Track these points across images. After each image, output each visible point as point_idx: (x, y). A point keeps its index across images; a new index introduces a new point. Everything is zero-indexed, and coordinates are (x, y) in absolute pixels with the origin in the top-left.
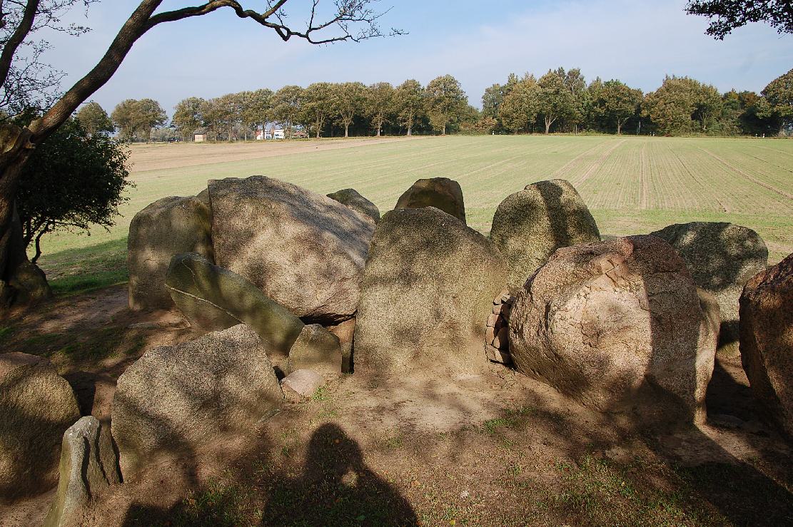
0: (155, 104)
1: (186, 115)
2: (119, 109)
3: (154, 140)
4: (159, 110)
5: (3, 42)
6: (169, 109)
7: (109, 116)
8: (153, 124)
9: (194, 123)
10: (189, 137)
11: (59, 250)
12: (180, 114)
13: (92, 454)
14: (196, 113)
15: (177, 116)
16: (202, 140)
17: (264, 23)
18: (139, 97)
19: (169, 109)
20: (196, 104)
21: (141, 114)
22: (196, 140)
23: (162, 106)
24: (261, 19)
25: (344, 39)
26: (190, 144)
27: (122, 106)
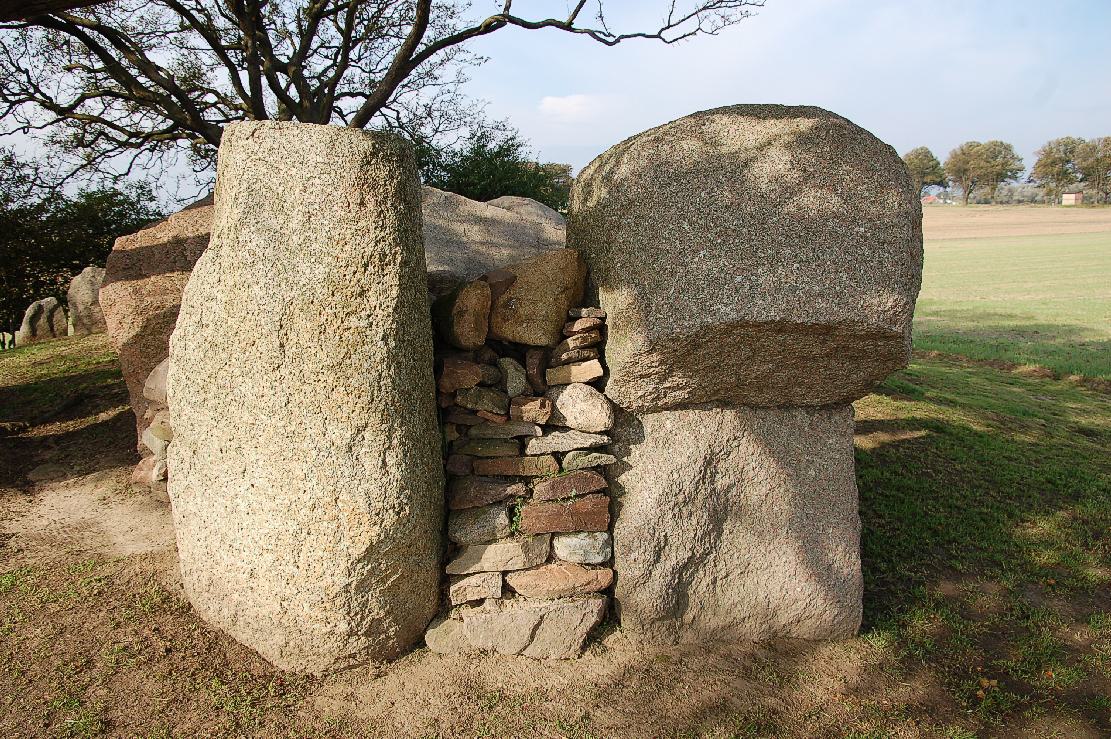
0: (1008, 148)
1: (1054, 163)
2: (954, 155)
3: (1019, 202)
4: (1013, 157)
5: (198, 3)
6: (1028, 158)
7: (941, 165)
8: (1001, 177)
9: (1063, 177)
10: (1054, 197)
11: (880, 416)
12: (1043, 162)
13: (421, 48)
14: (1068, 162)
15: (1040, 164)
16: (1073, 202)
17: (573, 30)
18: (984, 138)
19: (1028, 158)
20: (1070, 147)
21: (982, 163)
22: (1064, 203)
23: (1017, 151)
24: (568, 27)
25: (694, 33)
26: (1054, 208)
27: (959, 152)
